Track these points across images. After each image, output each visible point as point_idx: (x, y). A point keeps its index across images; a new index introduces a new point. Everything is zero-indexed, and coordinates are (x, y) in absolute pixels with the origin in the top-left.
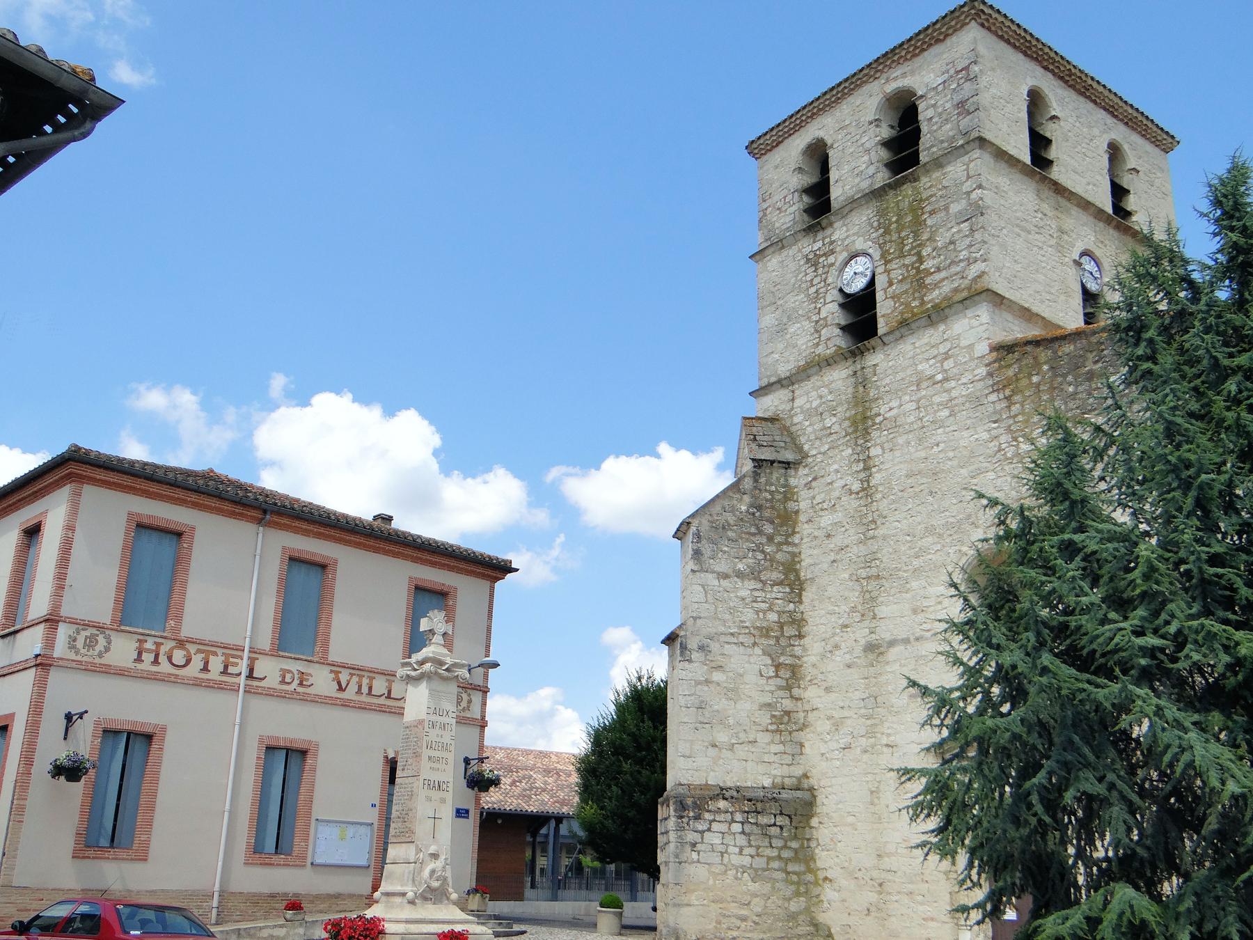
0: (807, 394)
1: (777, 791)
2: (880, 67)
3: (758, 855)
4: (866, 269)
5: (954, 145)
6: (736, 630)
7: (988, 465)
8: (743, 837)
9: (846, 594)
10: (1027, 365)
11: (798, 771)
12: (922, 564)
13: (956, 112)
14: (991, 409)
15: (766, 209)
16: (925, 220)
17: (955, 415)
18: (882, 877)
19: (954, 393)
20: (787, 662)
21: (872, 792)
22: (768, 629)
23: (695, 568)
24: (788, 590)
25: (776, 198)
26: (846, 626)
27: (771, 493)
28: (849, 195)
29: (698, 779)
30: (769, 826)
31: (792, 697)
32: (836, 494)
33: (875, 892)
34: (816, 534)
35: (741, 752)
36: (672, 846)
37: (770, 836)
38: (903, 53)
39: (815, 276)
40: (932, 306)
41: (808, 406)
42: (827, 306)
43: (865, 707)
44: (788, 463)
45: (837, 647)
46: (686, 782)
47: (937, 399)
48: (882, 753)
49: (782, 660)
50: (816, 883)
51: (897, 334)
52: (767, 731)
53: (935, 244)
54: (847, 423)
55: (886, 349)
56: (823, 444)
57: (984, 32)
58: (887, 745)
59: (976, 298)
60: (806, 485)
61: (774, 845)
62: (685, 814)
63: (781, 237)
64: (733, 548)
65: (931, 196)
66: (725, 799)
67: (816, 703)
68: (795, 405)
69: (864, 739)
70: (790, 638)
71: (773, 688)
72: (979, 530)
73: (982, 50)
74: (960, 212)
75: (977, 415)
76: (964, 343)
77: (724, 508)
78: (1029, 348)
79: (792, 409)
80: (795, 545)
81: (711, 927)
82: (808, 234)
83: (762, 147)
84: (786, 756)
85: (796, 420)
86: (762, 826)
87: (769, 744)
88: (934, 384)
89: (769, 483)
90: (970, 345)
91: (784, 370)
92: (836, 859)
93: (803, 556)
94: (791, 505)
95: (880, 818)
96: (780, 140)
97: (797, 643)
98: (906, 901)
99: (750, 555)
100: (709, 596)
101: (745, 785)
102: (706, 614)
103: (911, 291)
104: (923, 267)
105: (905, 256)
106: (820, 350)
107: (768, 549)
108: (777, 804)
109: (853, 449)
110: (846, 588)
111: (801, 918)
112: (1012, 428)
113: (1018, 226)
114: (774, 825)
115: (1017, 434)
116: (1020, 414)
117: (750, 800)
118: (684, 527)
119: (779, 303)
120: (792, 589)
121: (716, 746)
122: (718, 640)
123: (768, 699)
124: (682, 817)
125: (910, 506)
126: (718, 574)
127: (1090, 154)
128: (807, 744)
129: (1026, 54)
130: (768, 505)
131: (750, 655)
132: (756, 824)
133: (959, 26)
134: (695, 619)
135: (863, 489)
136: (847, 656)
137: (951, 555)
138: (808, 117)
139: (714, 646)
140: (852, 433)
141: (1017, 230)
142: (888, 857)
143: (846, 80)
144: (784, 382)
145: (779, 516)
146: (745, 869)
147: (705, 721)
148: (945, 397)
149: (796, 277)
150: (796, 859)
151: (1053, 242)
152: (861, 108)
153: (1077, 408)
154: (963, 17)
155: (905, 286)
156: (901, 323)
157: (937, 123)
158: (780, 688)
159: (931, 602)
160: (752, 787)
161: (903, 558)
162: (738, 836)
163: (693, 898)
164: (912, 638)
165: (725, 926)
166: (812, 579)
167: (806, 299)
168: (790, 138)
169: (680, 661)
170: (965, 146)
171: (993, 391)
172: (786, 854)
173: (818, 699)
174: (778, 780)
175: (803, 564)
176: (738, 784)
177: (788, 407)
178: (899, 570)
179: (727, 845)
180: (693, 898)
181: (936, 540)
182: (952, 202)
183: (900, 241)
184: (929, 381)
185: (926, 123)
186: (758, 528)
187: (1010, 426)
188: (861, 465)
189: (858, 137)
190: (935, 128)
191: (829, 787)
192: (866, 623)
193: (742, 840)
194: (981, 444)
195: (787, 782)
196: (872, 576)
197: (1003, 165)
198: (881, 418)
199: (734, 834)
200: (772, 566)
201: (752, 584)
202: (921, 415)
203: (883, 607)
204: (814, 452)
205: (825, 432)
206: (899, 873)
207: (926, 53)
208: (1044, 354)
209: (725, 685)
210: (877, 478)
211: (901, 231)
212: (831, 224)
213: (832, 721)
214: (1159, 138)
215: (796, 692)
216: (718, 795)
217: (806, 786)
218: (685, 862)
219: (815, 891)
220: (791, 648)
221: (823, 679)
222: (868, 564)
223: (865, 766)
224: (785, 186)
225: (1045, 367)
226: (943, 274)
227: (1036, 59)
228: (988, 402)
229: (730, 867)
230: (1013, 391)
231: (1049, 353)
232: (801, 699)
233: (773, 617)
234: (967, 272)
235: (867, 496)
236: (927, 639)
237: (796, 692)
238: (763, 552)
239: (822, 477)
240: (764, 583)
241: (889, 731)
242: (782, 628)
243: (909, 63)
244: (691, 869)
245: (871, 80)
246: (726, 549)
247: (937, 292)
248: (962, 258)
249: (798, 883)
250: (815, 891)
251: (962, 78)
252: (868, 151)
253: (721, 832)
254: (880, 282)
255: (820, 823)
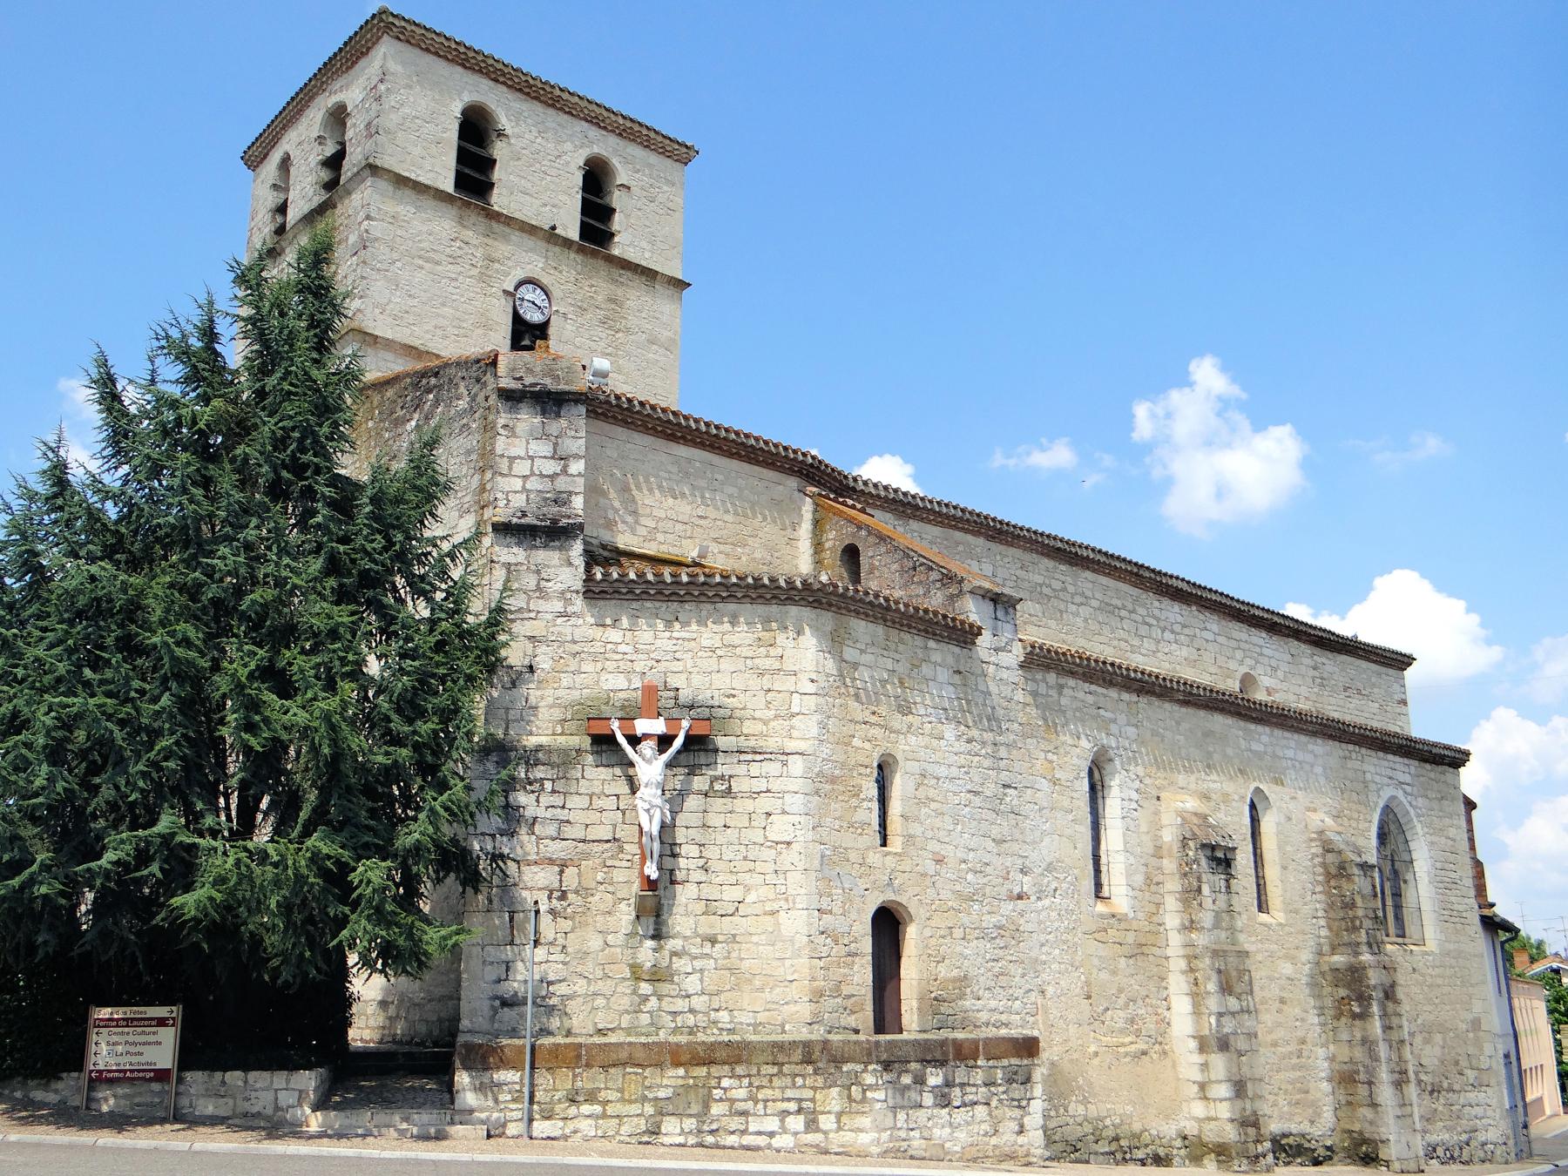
57: (400, 45)
73: (393, 66)
113: (420, 257)
127: (554, 172)
141: (421, 262)
151: (475, 272)
197: (408, 192)
214: (669, 148)
227: (480, 71)
243: (345, 76)
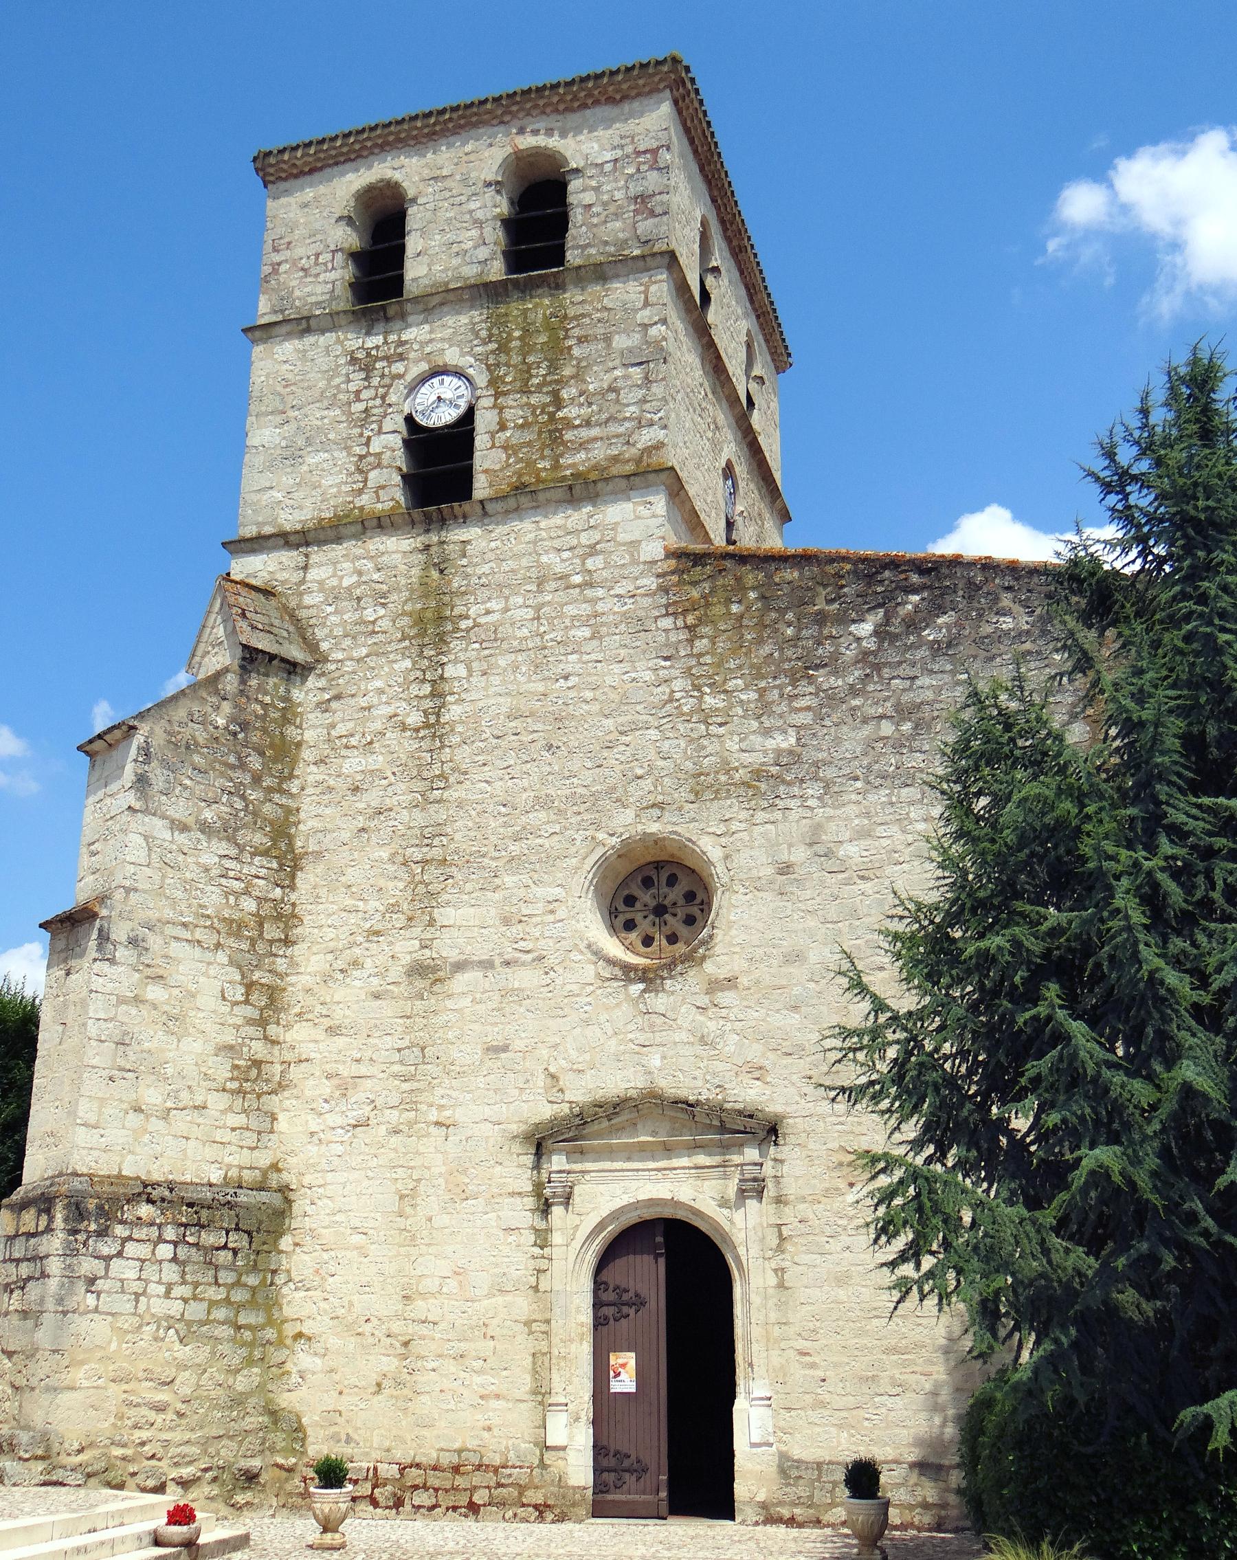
0: (335, 564)
1: (232, 1191)
2: (514, 108)
3: (195, 1298)
4: (459, 397)
5: (625, 253)
6: (191, 919)
7: (650, 718)
8: (174, 1267)
9: (382, 882)
10: (724, 586)
11: (264, 1160)
12: (526, 852)
13: (632, 207)
14: (661, 638)
15: (279, 264)
16: (570, 348)
17: (601, 638)
18: (410, 1331)
19: (600, 607)
20: (263, 981)
21: (402, 1197)
22: (241, 925)
23: (137, 805)
24: (275, 865)
25: (299, 251)
26: (377, 933)
27: (265, 706)
28: (439, 280)
29: (105, 1166)
30: (218, 1249)
31: (266, 1038)
32: (378, 726)
33: (395, 1356)
34: (332, 783)
35: (181, 1121)
36: (53, 1284)
37: (217, 1267)
38: (555, 99)
39: (365, 388)
40: (572, 474)
41: (334, 582)
42: (383, 436)
43: (401, 1062)
44: (294, 664)
45: (356, 964)
46: (85, 1171)
47: (571, 610)
48: (428, 1135)
49: (256, 976)
50: (280, 1343)
51: (512, 503)
52: (224, 1090)
53: (584, 387)
54: (406, 621)
55: (486, 521)
56: (357, 646)
58: (437, 1123)
59: (651, 477)
60: (319, 705)
61: (221, 1281)
62: (82, 1226)
63: (305, 314)
64: (199, 783)
65: (583, 316)
66: (150, 1201)
67: (306, 1050)
68: (309, 577)
69: (395, 1112)
70: (271, 942)
71: (240, 1021)
72: (627, 811)
74: (630, 350)
75: (638, 643)
76: (622, 537)
77: (191, 714)
78: (728, 564)
79: (303, 581)
80: (292, 796)
81: (107, 1425)
82: (358, 320)
83: (285, 166)
84: (248, 1134)
85: (308, 600)
86: (205, 1248)
87: (224, 1112)
88: (567, 588)
89: (261, 689)
90: (631, 542)
91: (290, 520)
92: (323, 1305)
93: (302, 815)
94: (291, 731)
95: (413, 1238)
96: (319, 165)
97: (281, 953)
98: (453, 1369)
99: (224, 800)
100: (153, 856)
101: (182, 1179)
102: (147, 886)
103: (537, 445)
104: (560, 414)
105: (531, 392)
106: (365, 500)
107: (253, 795)
108: (232, 1212)
109: (414, 663)
110: (382, 874)
111: (252, 1401)
112: (694, 671)
114: (225, 1247)
115: (701, 681)
116: (707, 653)
117: (191, 1205)
118: (118, 734)
119: (292, 414)
120: (281, 865)
121: (142, 1111)
122: (162, 933)
123: (229, 1038)
124: (75, 1232)
125: (512, 762)
126: (173, 822)
128: (281, 1117)
129: (702, 169)
130: (257, 725)
131: (209, 964)
132: (196, 1245)
133: (647, 89)
134: (128, 890)
135: (427, 725)
136: (375, 981)
137: (578, 843)
138: (376, 145)
139: (154, 941)
140: (413, 637)
142: (424, 1299)
143: (455, 109)
144: (292, 538)
145: (272, 746)
146: (172, 1322)
147: (128, 1067)
148: (585, 609)
149: (329, 380)
150: (252, 1304)
152: (472, 157)
153: (798, 659)
154: (656, 79)
155: (528, 436)
156: (517, 488)
157: (599, 214)
158: (250, 1022)
159: (539, 908)
160: (192, 1183)
161: (493, 838)
162: (165, 1265)
163: (79, 1375)
164: (497, 961)
165: (129, 1423)
166: (318, 855)
167: (344, 418)
168: (336, 168)
169: (95, 960)
170: (648, 259)
171: (667, 614)
172: (239, 1296)
173: (312, 1045)
174: (233, 1173)
175: (301, 827)
176: (171, 1177)
177: (296, 577)
178: (484, 856)
179: (147, 1282)
180: (81, 1375)
181: (553, 817)
182: (618, 333)
183: (525, 368)
184: (560, 582)
185: (579, 210)
186: (239, 758)
187: (690, 668)
188: (427, 689)
189: (464, 198)
190: (595, 220)
191: (319, 1186)
192: (417, 931)
193: (171, 1273)
194: (641, 688)
195: (248, 1176)
196: (433, 859)
198: (470, 623)
199: (161, 1262)
200: (255, 823)
201: (224, 847)
202: (542, 629)
203: (450, 911)
204: (340, 656)
205: (362, 628)
206: (442, 1326)
207: (588, 112)
208: (751, 577)
209: (166, 1008)
210: (454, 712)
211: (528, 353)
212: (403, 316)
213: (335, 1081)
215: (272, 1030)
216: (139, 1194)
217: (274, 1184)
218: (74, 1312)
219: (277, 1356)
220: (272, 959)
221: (324, 1012)
222: (427, 838)
223: (393, 1155)
224: (319, 237)
225: (752, 595)
226: (595, 432)
228: (658, 629)
229: (147, 1318)
230: (699, 619)
231: (761, 575)
232: (278, 1043)
233: (249, 905)
234: (635, 437)
235: (434, 736)
236: (523, 964)
237: (272, 1030)
238: (243, 797)
239: (353, 696)
240: (241, 849)
241: (443, 1102)
242: (261, 925)
243: (560, 117)
244: (81, 1324)
245: (495, 122)
246: (188, 782)
247: (583, 455)
248: (628, 415)
249: (251, 1345)
250: (277, 1356)
251: (644, 163)
252: (479, 224)
253: (138, 1259)
254: (484, 421)
255: (297, 1244)
